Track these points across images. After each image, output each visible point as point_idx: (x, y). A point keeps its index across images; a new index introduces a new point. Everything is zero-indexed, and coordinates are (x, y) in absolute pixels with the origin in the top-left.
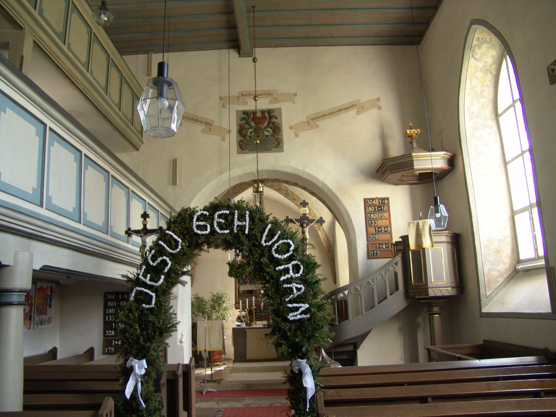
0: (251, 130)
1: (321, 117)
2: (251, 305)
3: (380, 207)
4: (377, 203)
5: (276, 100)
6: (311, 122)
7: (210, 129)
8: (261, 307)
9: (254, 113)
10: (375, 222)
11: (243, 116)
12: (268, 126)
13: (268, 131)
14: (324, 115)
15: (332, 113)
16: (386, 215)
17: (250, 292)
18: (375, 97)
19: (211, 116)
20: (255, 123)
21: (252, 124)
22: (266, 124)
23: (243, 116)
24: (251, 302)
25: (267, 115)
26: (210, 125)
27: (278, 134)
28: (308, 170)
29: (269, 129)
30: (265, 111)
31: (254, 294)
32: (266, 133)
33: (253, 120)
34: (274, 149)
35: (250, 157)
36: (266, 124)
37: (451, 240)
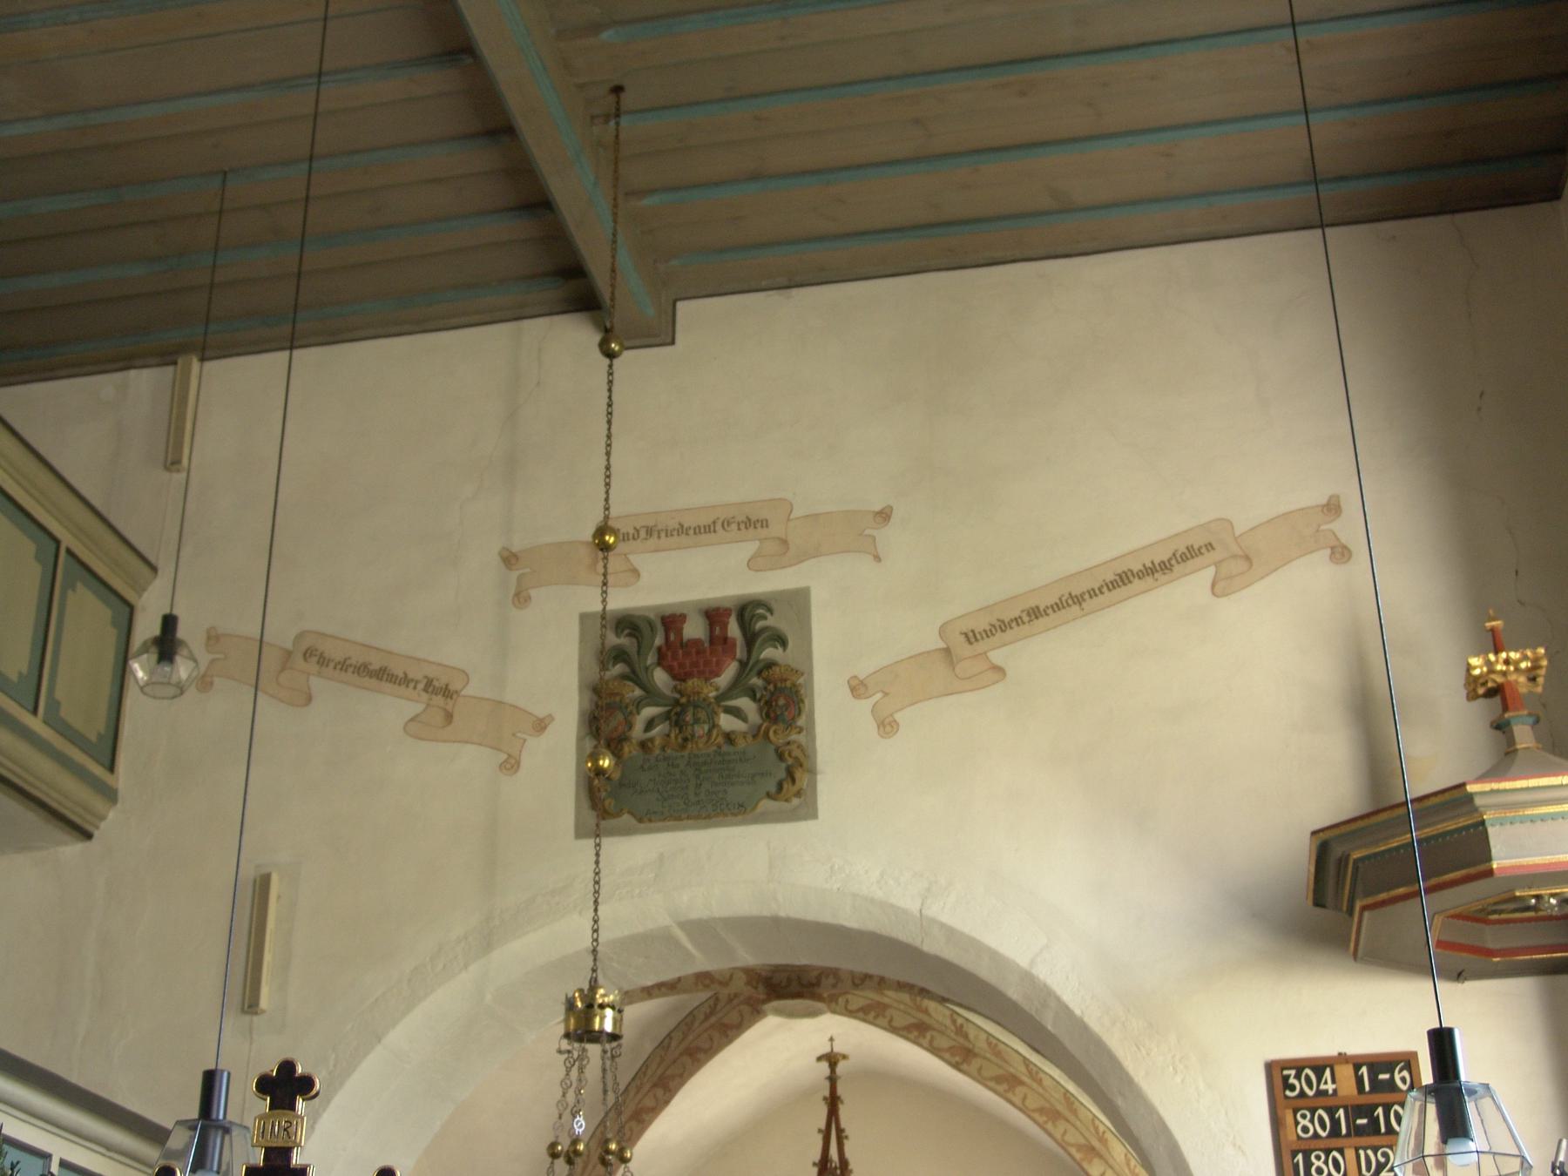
0: (649, 712)
1: (1018, 621)
3: (1368, 1111)
4: (1347, 1087)
5: (783, 552)
6: (962, 648)
7: (449, 717)
9: (671, 621)
12: (736, 687)
13: (737, 713)
14: (1035, 613)
15: (1078, 600)
18: (1315, 496)
19: (456, 652)
20: (669, 670)
21: (660, 677)
25: (734, 630)
26: (447, 693)
27: (790, 725)
29: (744, 703)
30: (727, 612)
32: (726, 722)
33: (661, 660)
34: (766, 804)
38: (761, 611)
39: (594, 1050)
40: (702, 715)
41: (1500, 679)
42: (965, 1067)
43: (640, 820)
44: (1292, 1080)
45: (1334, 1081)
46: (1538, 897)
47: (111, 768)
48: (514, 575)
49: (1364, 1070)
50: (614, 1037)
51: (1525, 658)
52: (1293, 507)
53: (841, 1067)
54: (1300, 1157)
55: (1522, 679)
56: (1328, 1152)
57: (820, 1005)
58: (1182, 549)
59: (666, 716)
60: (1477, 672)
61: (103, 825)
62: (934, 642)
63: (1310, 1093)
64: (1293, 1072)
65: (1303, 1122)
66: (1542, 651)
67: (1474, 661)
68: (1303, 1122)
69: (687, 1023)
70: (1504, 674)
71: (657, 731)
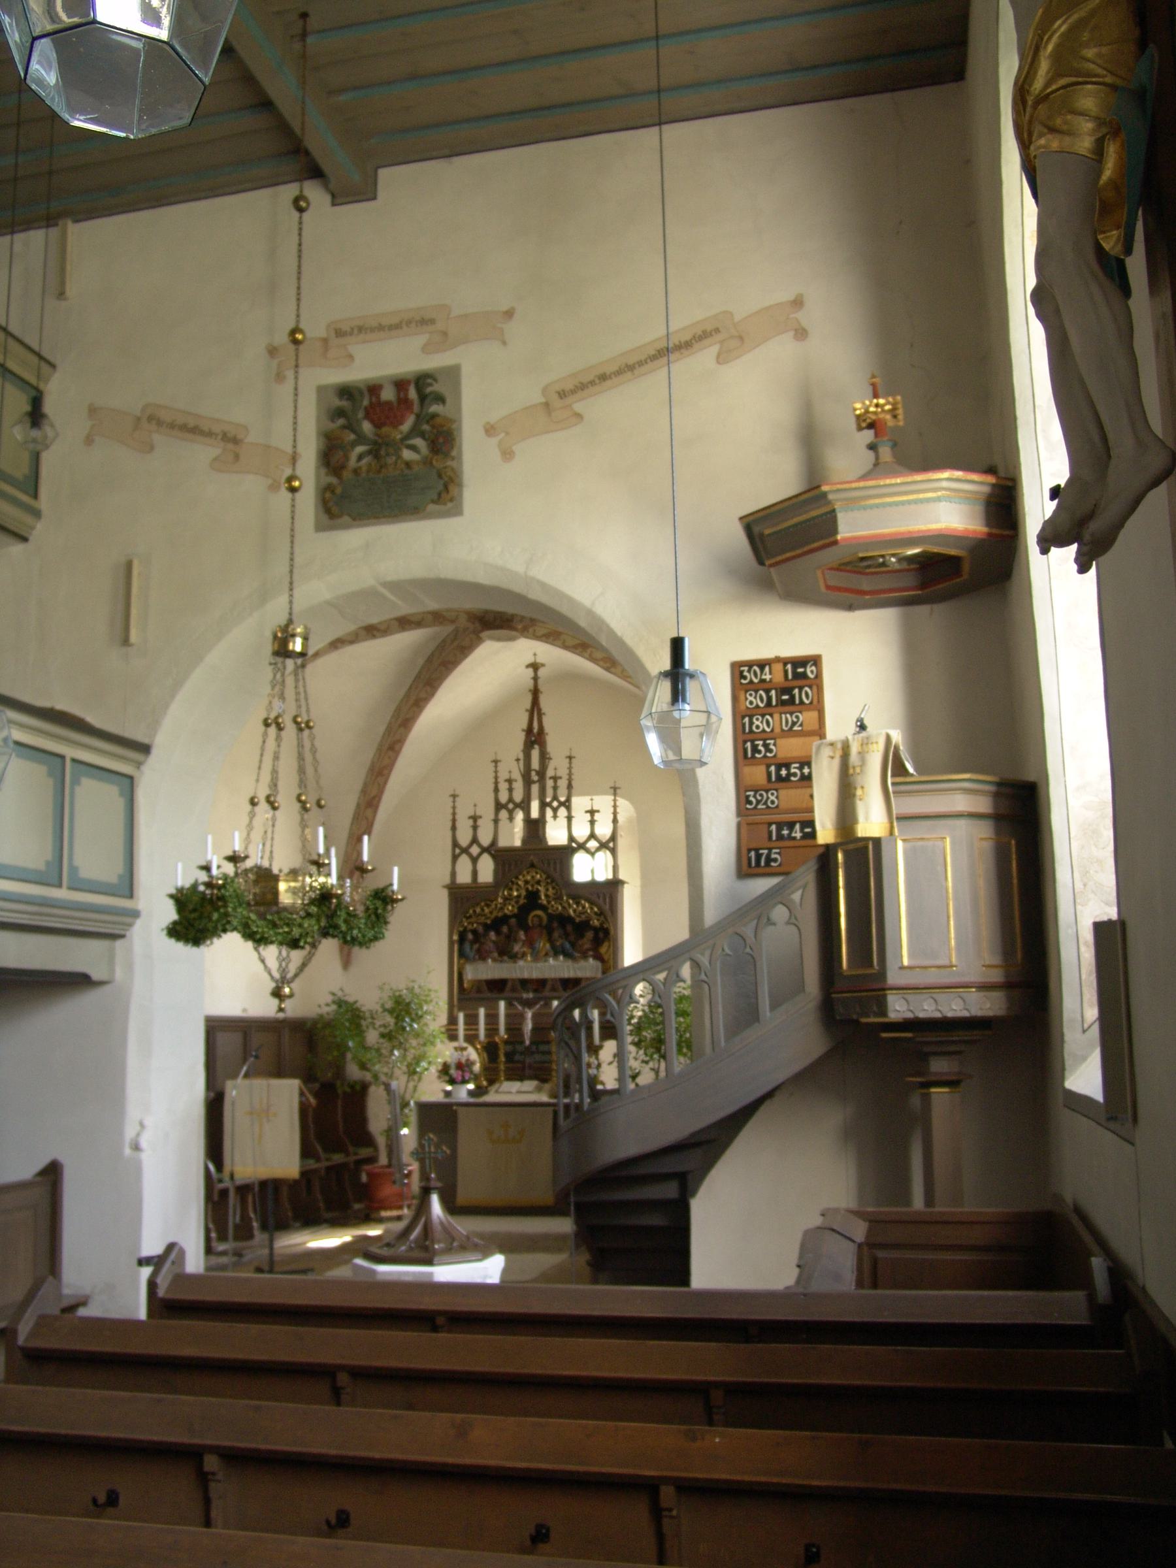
0: (360, 449)
1: (592, 383)
2: (492, 1030)
3: (788, 690)
4: (778, 677)
5: (444, 341)
6: (557, 403)
7: (237, 457)
8: (522, 1035)
9: (374, 389)
10: (766, 746)
11: (337, 402)
12: (415, 431)
13: (413, 448)
14: (603, 377)
15: (631, 368)
16: (807, 718)
17: (497, 986)
18: (786, 296)
19: (240, 413)
20: (372, 422)
21: (367, 427)
22: (406, 426)
23: (337, 402)
24: (492, 1018)
25: (412, 394)
26: (235, 441)
27: (447, 455)
28: (540, 572)
29: (419, 442)
30: (409, 382)
31: (507, 994)
32: (407, 455)
33: (368, 416)
34: (431, 507)
35: (355, 538)
36: (406, 426)
37: (996, 805)
38: (429, 381)
39: (290, 664)
40: (391, 450)
41: (874, 417)
42: (613, 670)
43: (354, 519)
44: (746, 673)
45: (770, 673)
46: (883, 556)
47: (35, 496)
48: (275, 363)
49: (789, 667)
50: (302, 654)
51: (888, 403)
52: (772, 303)
53: (542, 672)
54: (747, 720)
55: (888, 417)
56: (763, 716)
57: (514, 633)
58: (700, 333)
59: (369, 452)
60: (858, 412)
61: (34, 532)
62: (539, 399)
63: (756, 681)
64: (746, 669)
65: (750, 698)
66: (899, 398)
67: (858, 405)
68: (750, 698)
69: (442, 646)
70: (875, 413)
71: (365, 461)
